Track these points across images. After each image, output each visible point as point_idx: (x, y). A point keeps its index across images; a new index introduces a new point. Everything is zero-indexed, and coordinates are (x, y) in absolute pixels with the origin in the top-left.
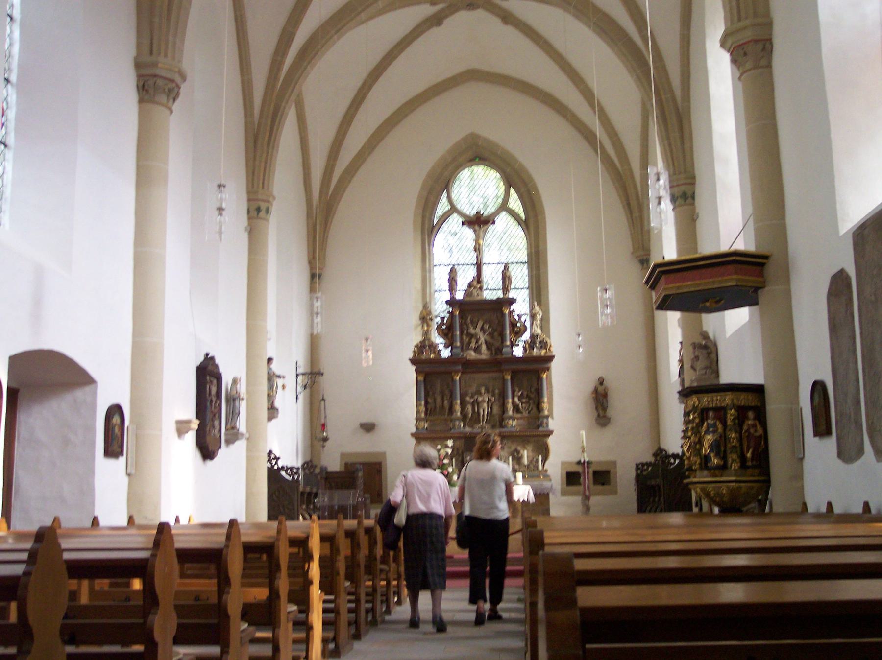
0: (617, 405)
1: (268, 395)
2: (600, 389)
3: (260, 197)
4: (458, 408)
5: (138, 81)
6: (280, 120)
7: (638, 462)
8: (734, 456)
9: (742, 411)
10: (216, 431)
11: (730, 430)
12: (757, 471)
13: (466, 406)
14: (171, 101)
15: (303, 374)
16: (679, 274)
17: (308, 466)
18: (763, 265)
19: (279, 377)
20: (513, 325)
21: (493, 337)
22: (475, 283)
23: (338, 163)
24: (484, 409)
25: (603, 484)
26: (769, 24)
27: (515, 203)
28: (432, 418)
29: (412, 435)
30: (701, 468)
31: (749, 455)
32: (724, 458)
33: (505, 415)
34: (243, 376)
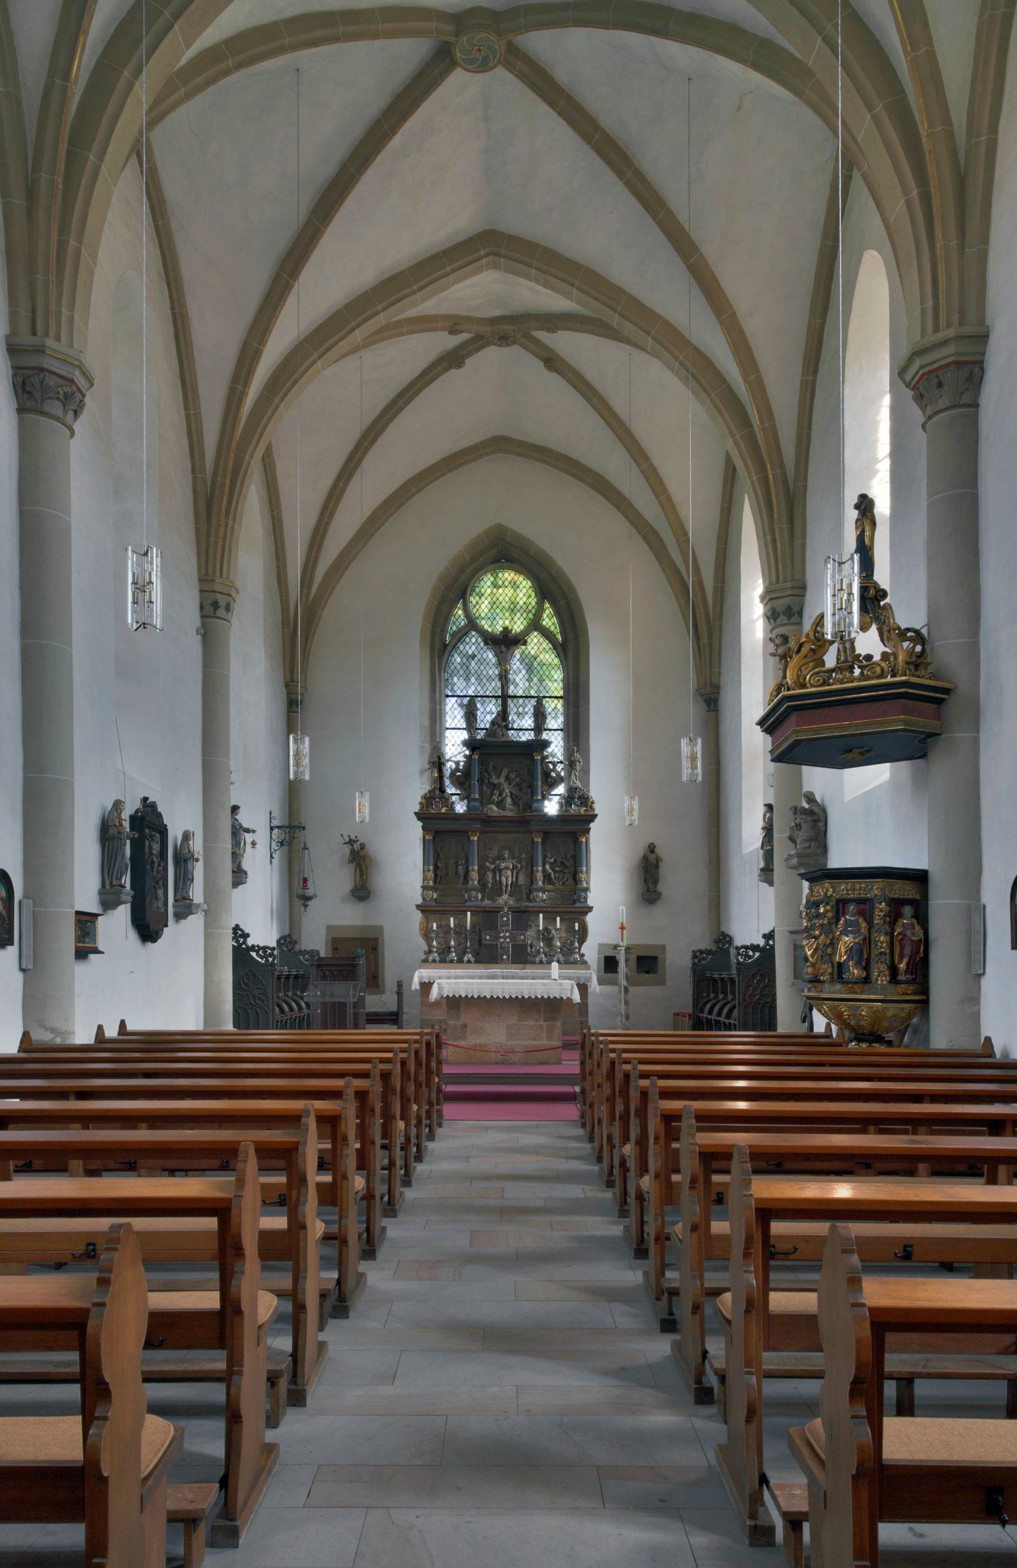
0: (670, 881)
1: (233, 853)
2: (652, 857)
3: (217, 588)
4: (475, 875)
5: (14, 376)
6: (243, 482)
7: (695, 949)
8: (883, 967)
9: (896, 906)
10: (160, 904)
11: (879, 931)
12: (912, 988)
13: (485, 874)
14: (71, 413)
15: (278, 827)
16: (818, 711)
17: (287, 941)
18: (939, 702)
19: (248, 831)
20: (546, 774)
21: (520, 789)
22: (500, 721)
23: (324, 554)
24: (507, 878)
25: (648, 972)
26: (983, 338)
27: (549, 620)
28: (442, 887)
29: (418, 907)
30: (832, 981)
31: (902, 966)
32: (867, 968)
33: (534, 886)
34: (196, 826)
